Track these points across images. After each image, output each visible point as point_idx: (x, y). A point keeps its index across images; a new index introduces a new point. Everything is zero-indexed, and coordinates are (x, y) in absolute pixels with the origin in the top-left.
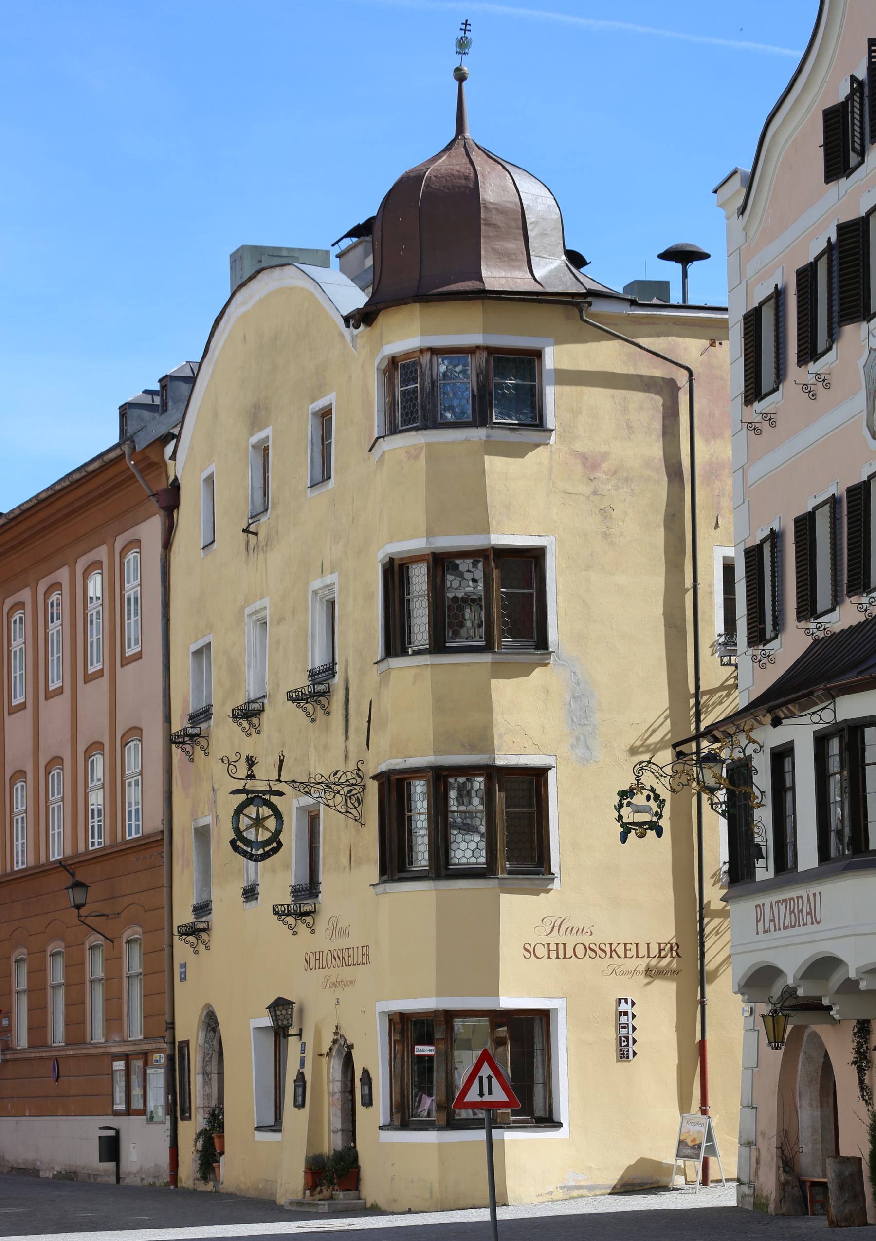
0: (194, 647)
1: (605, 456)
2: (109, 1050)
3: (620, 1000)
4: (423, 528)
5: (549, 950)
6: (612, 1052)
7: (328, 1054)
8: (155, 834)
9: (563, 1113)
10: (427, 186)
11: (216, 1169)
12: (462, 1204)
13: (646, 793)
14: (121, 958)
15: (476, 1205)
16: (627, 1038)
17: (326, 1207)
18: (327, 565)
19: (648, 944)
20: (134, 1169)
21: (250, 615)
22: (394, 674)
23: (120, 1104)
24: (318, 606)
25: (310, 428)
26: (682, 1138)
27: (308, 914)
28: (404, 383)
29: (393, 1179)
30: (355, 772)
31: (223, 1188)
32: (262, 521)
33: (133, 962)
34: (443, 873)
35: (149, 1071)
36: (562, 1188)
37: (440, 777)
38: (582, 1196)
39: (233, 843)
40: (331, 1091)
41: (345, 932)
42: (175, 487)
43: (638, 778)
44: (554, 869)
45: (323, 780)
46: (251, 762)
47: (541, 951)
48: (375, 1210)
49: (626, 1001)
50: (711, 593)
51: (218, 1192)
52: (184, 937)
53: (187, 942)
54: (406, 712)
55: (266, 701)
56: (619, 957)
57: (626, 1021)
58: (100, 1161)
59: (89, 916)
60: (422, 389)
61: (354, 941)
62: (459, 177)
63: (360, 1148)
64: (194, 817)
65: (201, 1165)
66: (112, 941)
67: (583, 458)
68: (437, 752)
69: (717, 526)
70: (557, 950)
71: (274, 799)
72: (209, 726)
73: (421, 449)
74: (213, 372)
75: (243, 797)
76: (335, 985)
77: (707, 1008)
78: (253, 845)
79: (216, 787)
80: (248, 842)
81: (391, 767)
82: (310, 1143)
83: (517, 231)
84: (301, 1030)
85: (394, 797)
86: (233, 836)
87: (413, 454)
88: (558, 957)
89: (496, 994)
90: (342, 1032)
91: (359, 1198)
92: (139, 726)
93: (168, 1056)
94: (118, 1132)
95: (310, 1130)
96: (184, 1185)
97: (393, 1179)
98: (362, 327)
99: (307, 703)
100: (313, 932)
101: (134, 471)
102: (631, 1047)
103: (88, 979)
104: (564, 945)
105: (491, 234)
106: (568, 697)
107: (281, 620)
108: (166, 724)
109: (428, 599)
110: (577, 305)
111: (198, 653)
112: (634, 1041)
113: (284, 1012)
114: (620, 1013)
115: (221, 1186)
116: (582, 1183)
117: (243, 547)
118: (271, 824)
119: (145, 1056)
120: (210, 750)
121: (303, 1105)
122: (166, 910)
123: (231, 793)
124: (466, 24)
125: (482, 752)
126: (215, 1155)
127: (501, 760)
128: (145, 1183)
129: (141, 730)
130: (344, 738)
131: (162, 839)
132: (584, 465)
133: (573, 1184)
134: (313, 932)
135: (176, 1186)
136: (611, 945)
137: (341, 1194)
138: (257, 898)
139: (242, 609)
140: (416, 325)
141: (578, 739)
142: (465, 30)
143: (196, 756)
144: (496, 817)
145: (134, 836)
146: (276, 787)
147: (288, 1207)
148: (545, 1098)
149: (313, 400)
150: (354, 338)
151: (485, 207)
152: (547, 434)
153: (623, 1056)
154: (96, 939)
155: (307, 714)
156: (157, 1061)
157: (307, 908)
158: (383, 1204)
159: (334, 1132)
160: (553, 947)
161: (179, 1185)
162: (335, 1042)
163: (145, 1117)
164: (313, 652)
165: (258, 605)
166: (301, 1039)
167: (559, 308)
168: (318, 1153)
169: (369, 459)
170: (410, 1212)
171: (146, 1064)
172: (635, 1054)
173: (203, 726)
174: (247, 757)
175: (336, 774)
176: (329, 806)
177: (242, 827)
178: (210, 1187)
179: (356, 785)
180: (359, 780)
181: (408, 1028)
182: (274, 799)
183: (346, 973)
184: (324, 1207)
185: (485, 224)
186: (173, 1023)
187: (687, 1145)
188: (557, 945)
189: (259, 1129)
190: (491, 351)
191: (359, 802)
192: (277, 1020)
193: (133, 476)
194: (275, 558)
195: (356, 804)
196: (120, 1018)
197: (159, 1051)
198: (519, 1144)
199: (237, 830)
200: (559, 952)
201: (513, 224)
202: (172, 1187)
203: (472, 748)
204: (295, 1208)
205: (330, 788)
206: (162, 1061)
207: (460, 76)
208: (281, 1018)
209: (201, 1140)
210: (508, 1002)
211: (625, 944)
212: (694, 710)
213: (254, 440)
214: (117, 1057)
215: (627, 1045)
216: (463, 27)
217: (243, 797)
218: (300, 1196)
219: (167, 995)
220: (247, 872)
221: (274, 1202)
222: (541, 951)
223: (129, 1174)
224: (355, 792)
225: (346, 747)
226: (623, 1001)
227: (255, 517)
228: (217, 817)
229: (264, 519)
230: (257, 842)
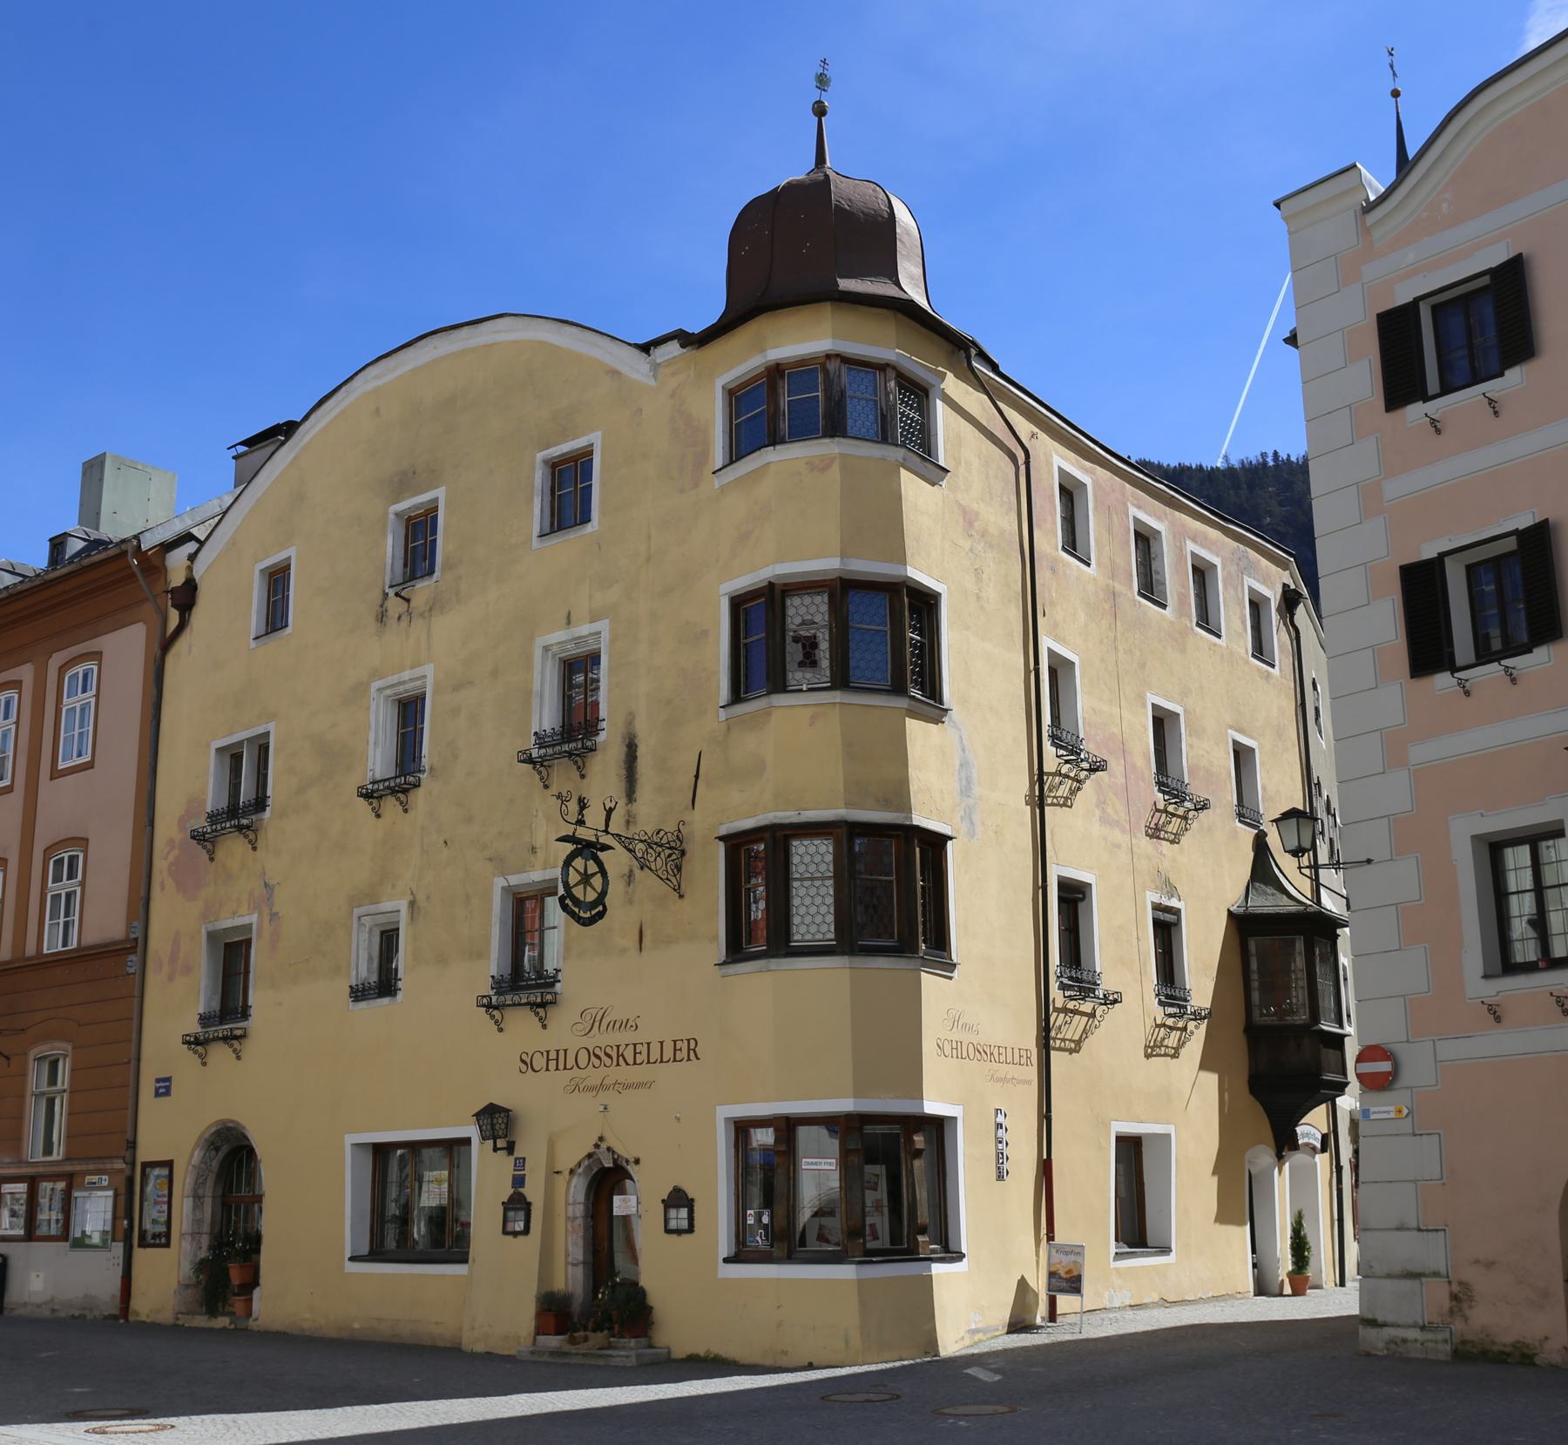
7: (572, 1172)
17: (633, 1360)
21: (380, 690)
24: (549, 664)
29: (779, 1324)
46: (582, 804)
47: (539, 1062)
51: (246, 1329)
54: (793, 759)
73: (833, 460)
75: (570, 847)
80: (576, 901)
82: (541, 1279)
91: (651, 1346)
97: (779, 1324)
101: (136, 570)
118: (597, 881)
120: (259, 844)
135: (127, 1320)
146: (605, 839)
160: (553, 1055)
161: (131, 1318)
162: (590, 1156)
163: (67, 1244)
170: (810, 1367)
177: (572, 881)
189: (352, 1259)
191: (679, 869)
203: (886, 804)
207: (820, 111)
209: (998, 1378)
217: (570, 847)
219: (130, 1112)
222: (539, 1062)
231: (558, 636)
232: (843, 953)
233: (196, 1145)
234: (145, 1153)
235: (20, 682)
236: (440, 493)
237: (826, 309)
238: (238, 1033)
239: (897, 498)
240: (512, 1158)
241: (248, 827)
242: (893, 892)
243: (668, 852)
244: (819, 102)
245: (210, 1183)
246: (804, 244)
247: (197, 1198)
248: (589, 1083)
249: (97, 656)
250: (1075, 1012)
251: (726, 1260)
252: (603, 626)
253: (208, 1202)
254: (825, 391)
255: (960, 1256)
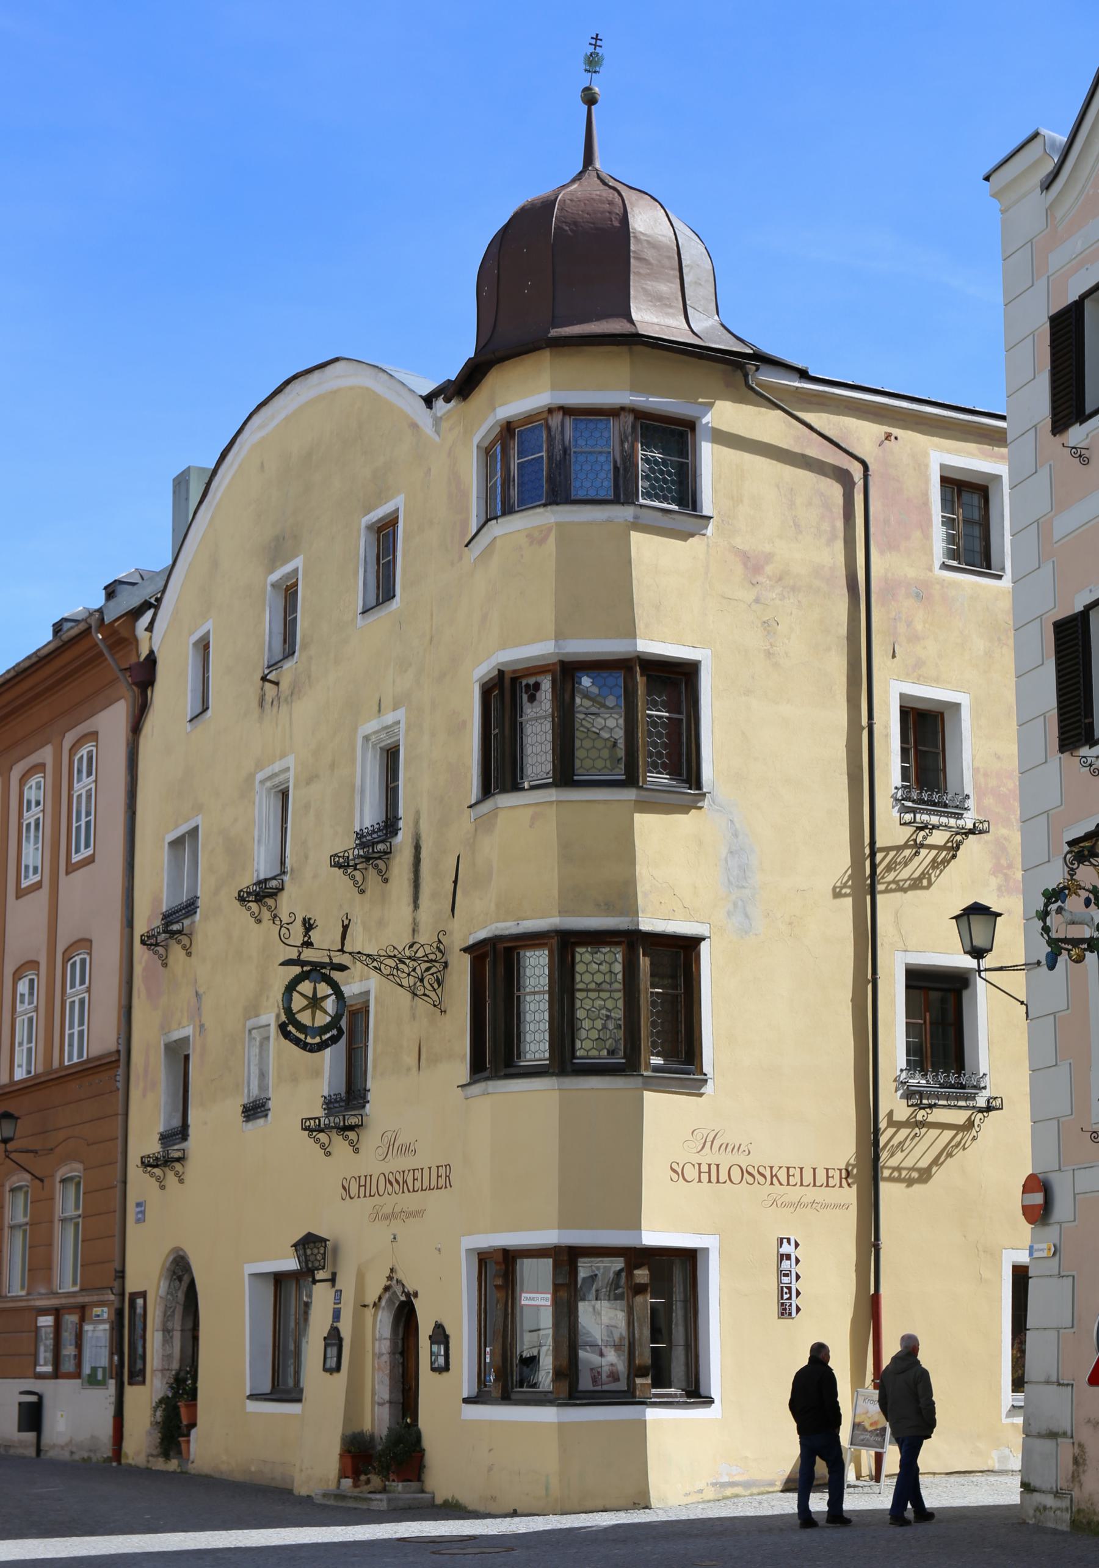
0: (172, 836)
1: (769, 557)
2: (32, 1303)
3: (782, 1239)
4: (551, 628)
5: (700, 1172)
6: (774, 1308)
7: (375, 1305)
8: (110, 1054)
9: (716, 1383)
10: (561, 209)
11: (184, 1446)
12: (589, 1505)
13: (1084, 894)
14: (52, 1199)
15: (608, 1507)
16: (789, 1289)
17: (385, 1503)
18: (387, 702)
19: (814, 1169)
20: (62, 1440)
21: (262, 782)
22: (502, 816)
23: (45, 1364)
24: (370, 755)
25: (362, 545)
26: (857, 1420)
27: (351, 1128)
28: (521, 454)
29: (490, 1469)
30: (435, 945)
31: (192, 1468)
32: (285, 667)
33: (66, 1204)
34: (569, 1068)
35: (87, 1327)
36: (714, 1484)
37: (565, 944)
38: (737, 1496)
39: (282, 1027)
40: (377, 1351)
41: (408, 1150)
42: (151, 660)
43: (1072, 872)
44: (706, 1069)
45: (396, 952)
46: (308, 926)
47: (691, 1173)
48: (453, 1510)
49: (789, 1240)
50: (887, 736)
51: (186, 1473)
52: (149, 1169)
53: (152, 1175)
54: (511, 866)
55: (286, 878)
56: (781, 1184)
57: (788, 1267)
58: (20, 1430)
59: (15, 1151)
60: (550, 458)
61: (425, 1159)
62: (602, 202)
63: (423, 1423)
64: (165, 1028)
65: (162, 1440)
66: (42, 1180)
67: (745, 557)
68: (562, 912)
69: (894, 656)
70: (709, 1172)
71: (336, 975)
72: (193, 922)
73: (550, 529)
74: (212, 517)
75: (296, 970)
76: (390, 1217)
77: (882, 1252)
78: (309, 1031)
79: (201, 991)
81: (498, 933)
82: (348, 1419)
83: (672, 272)
84: (334, 1275)
85: (501, 970)
86: (283, 1018)
87: (537, 538)
88: (710, 1181)
89: (637, 1226)
90: (399, 1275)
91: (423, 1491)
92: (88, 937)
93: (116, 1310)
94: (40, 1397)
95: (347, 1402)
96: (130, 1461)
97: (490, 1469)
98: (453, 403)
99: (355, 869)
100: (356, 1151)
101: (101, 645)
102: (794, 1301)
103: (6, 1224)
104: (718, 1166)
105: (641, 271)
106: (724, 851)
107: (311, 779)
108: (127, 930)
109: (553, 721)
110: (741, 367)
111: (177, 844)
112: (798, 1293)
113: (316, 1251)
114: (782, 1255)
115: (190, 1466)
116: (736, 1479)
117: (255, 704)
119: (82, 1311)
120: (193, 950)
121: (338, 1369)
122: (120, 1141)
123: (282, 964)
124: (596, 39)
125: (622, 914)
126: (179, 1427)
127: (648, 924)
128: (76, 1457)
129: (91, 941)
130: (411, 907)
131: (118, 1061)
132: (745, 565)
133: (725, 1479)
134: (356, 1151)
136: (771, 1168)
137: (400, 1486)
138: (266, 1116)
139: (251, 777)
140: (546, 378)
141: (735, 905)
142: (595, 45)
143: (171, 960)
144: (639, 997)
145: (75, 1060)
146: (338, 959)
147: (319, 1500)
148: (687, 1365)
149: (368, 510)
150: (437, 422)
151: (635, 237)
152: (704, 522)
153: (785, 1312)
154: (22, 1179)
155: (355, 883)
156: (98, 1316)
157: (353, 1121)
158: (468, 1499)
159: (380, 1404)
160: (704, 1168)
161: (123, 1461)
162: (387, 1289)
163: (79, 1381)
164: (362, 810)
165: (277, 767)
166: (333, 1286)
167: (721, 366)
168: (357, 1430)
169: (461, 558)
170: (515, 1514)
171: (82, 1319)
172: (798, 1309)
173: (187, 922)
174: (304, 919)
175: (411, 946)
176: (402, 986)
178: (173, 1465)
179: (435, 961)
180: (439, 955)
181: (499, 1269)
182: (336, 975)
183: (410, 1201)
184: (380, 1502)
185: (635, 258)
186: (123, 1272)
187: (865, 1430)
188: (709, 1165)
189: (252, 1397)
190: (641, 416)
191: (440, 983)
192: (307, 1262)
193: (101, 654)
194: (304, 709)
195: (436, 986)
196: (49, 1268)
197: (101, 1304)
198: (665, 1423)
199: (288, 1011)
200: (711, 1174)
201: (666, 262)
202: (114, 1464)
203: (609, 908)
204: (332, 1502)
205: (404, 963)
206: (106, 1316)
207: (590, 99)
208: (312, 1258)
210: (652, 1237)
211: (788, 1168)
212: (869, 882)
213: (275, 577)
214: (44, 1312)
215: (790, 1298)
216: (593, 42)
217: (296, 970)
218: (332, 1486)
220: (249, 1086)
221: (290, 1492)
222: (691, 1173)
223: (54, 1446)
224: (433, 970)
225: (414, 919)
226: (785, 1241)
227: (273, 666)
228: (202, 1026)
229: (288, 665)
230: (313, 1028)
231: (371, 726)
232: (553, 1074)
233: (161, 1276)
234: (131, 1286)
235: (43, 765)
236: (298, 562)
237: (545, 357)
238: (177, 1155)
239: (626, 562)
240: (334, 1290)
241: (180, 932)
242: (644, 1006)
243: (424, 966)
244: (587, 90)
245: (178, 1317)
246: (554, 275)
247: (166, 1331)
248: (785, 1199)
249: (93, 736)
250: (922, 1124)
251: (466, 1401)
252: (400, 714)
253: (177, 1335)
254: (548, 451)
255: (709, 1401)
